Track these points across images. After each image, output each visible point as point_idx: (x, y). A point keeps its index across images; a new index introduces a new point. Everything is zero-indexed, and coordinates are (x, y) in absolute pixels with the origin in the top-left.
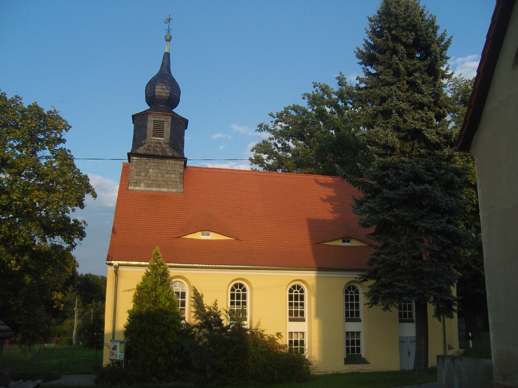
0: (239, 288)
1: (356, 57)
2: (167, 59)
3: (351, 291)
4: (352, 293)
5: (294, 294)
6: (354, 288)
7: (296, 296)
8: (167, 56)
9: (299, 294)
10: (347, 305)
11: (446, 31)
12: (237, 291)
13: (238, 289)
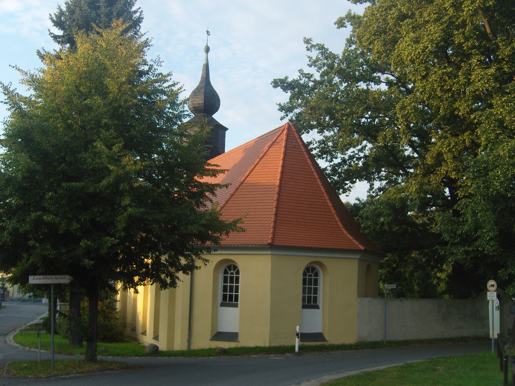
1: (37, 54)
3: (310, 273)
4: (310, 275)
6: (313, 269)
7: (232, 278)
8: (207, 68)
10: (304, 289)
11: (143, 12)
13: (232, 271)
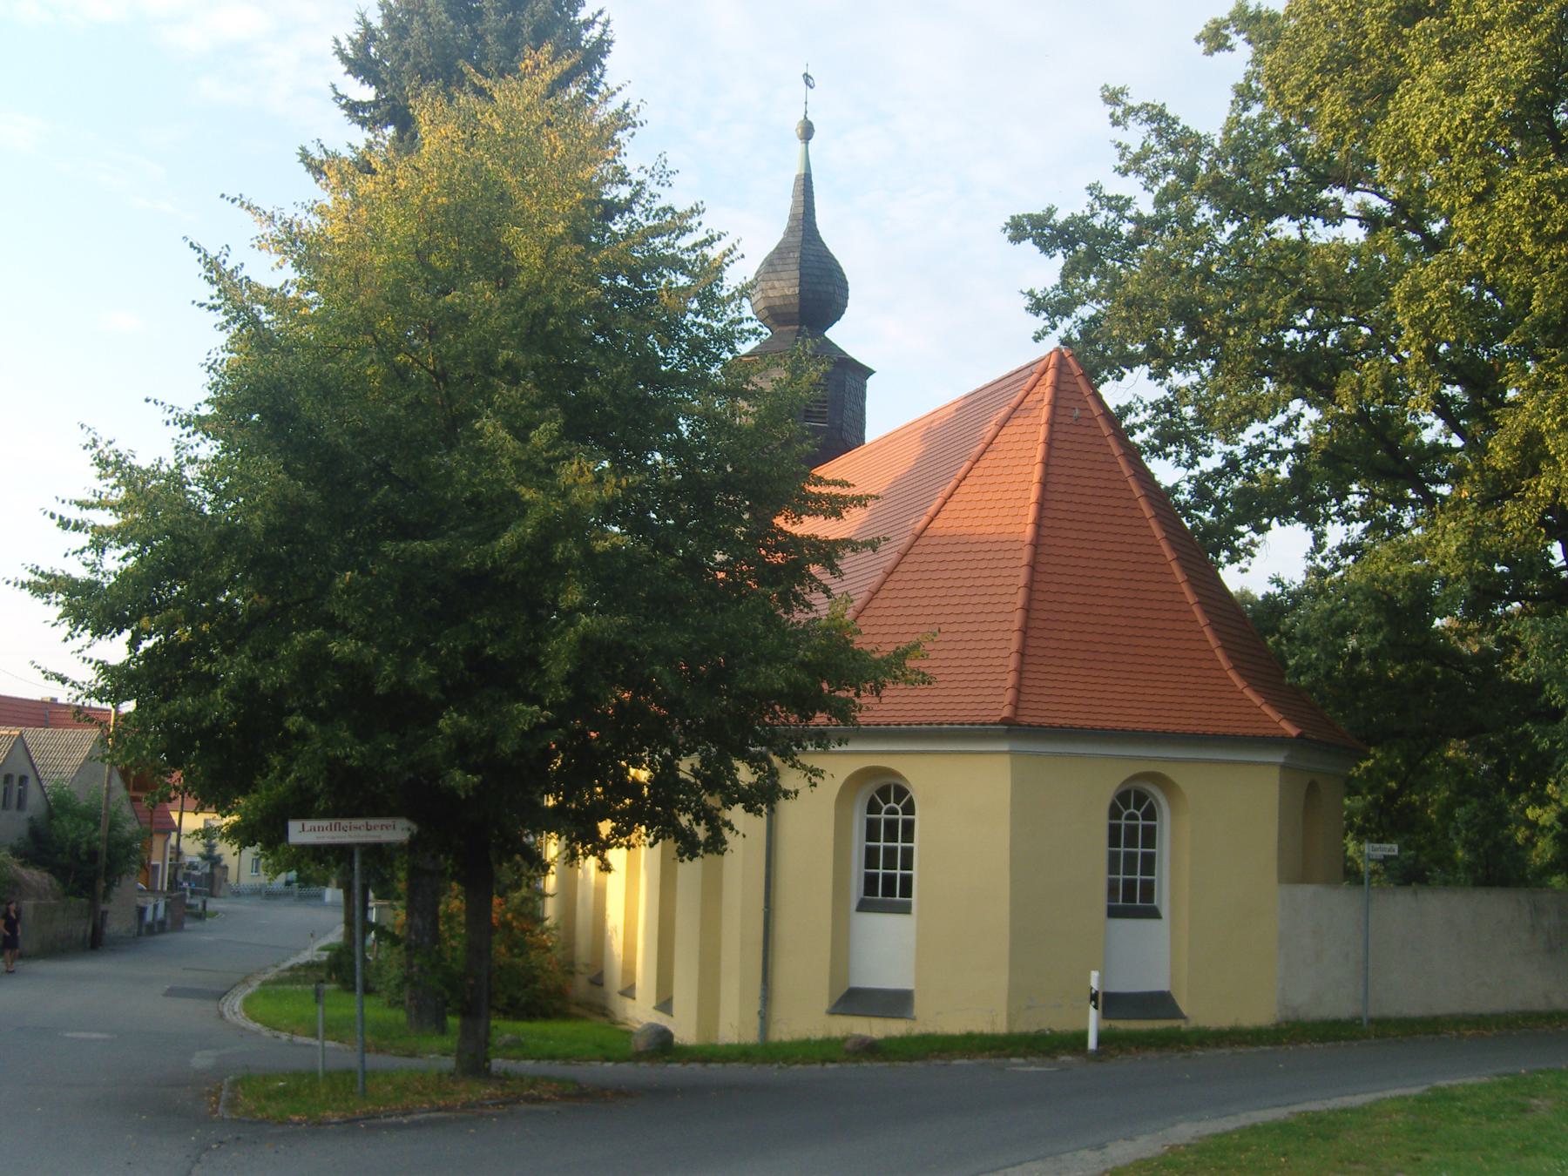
0: (1135, 808)
2: (1098, 223)
3: (1132, 810)
4: (1132, 817)
5: (883, 816)
6: (1141, 798)
7: (891, 826)
9: (900, 817)
10: (1113, 860)
12: (886, 813)
13: (892, 804)
